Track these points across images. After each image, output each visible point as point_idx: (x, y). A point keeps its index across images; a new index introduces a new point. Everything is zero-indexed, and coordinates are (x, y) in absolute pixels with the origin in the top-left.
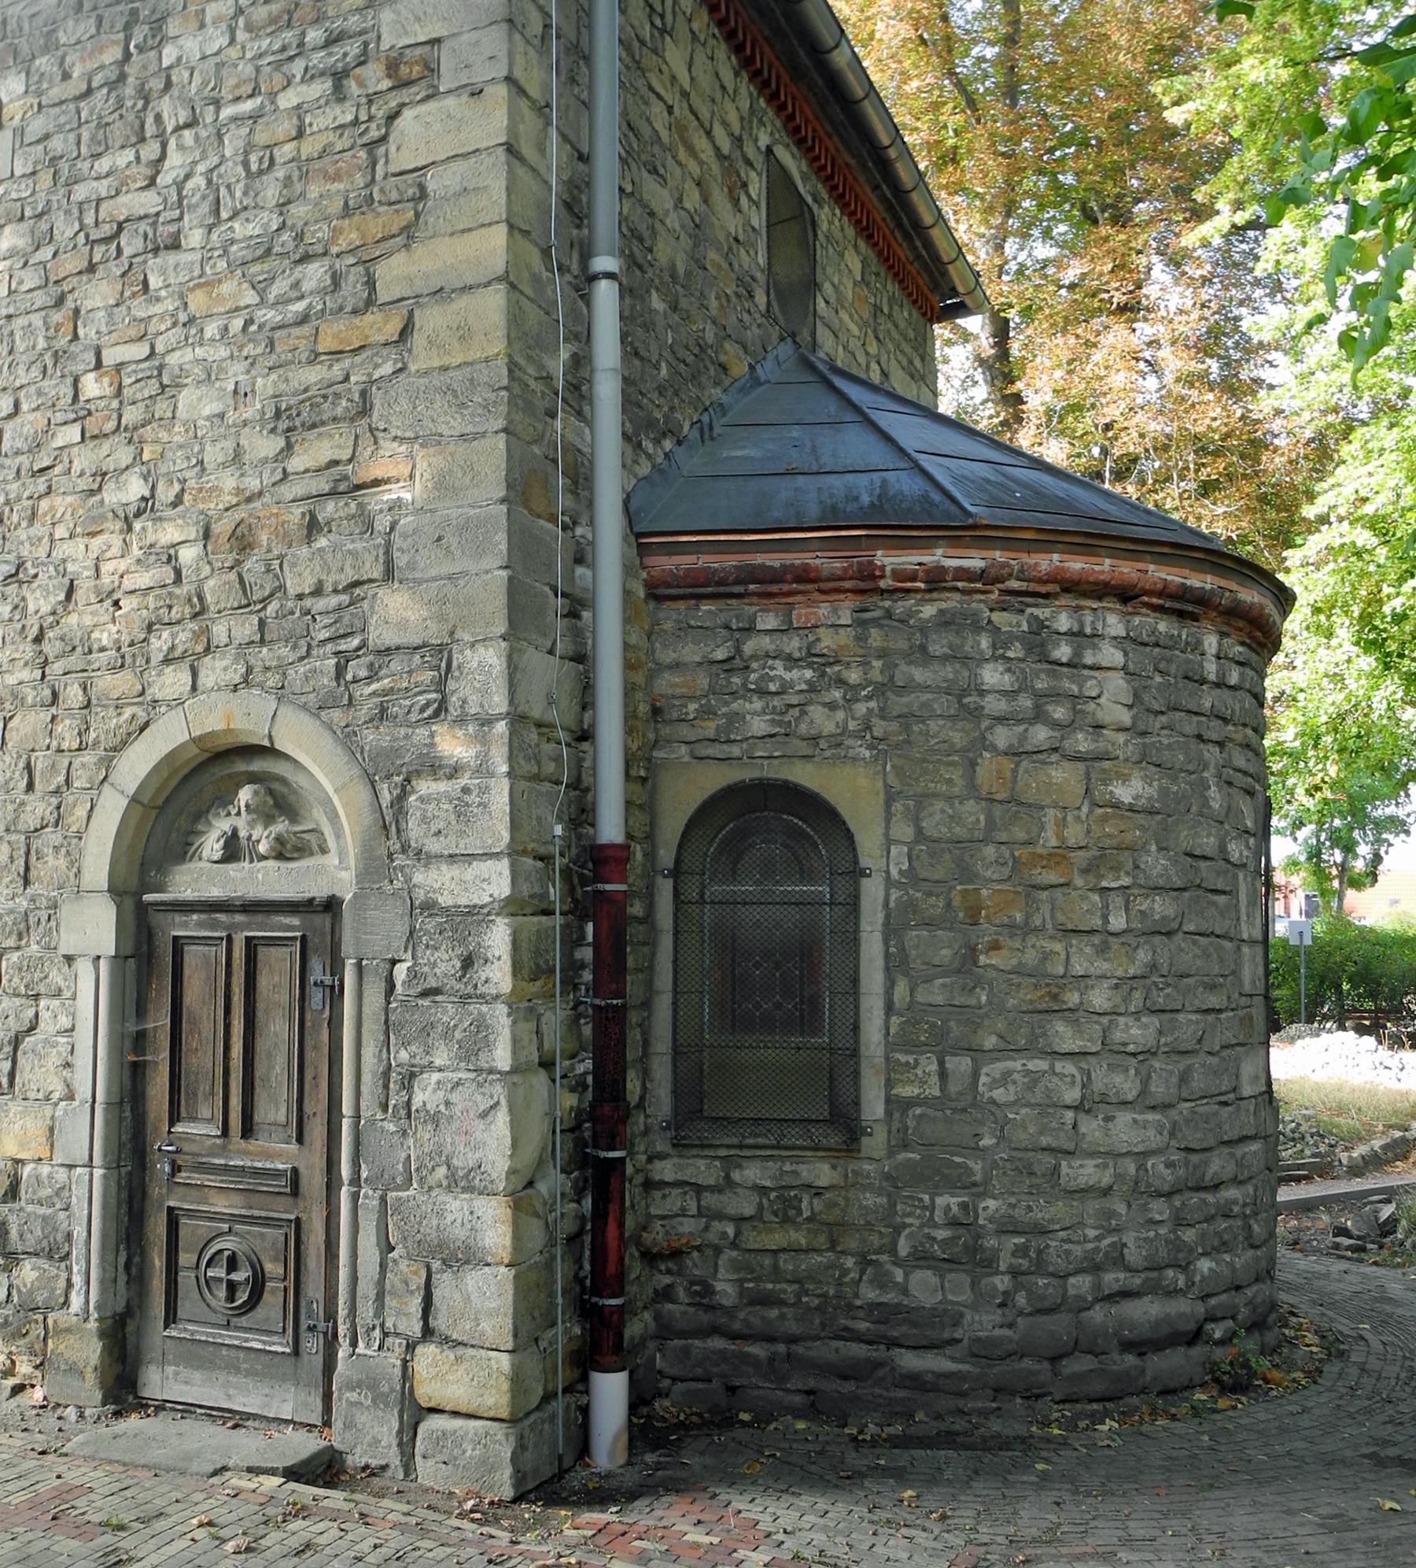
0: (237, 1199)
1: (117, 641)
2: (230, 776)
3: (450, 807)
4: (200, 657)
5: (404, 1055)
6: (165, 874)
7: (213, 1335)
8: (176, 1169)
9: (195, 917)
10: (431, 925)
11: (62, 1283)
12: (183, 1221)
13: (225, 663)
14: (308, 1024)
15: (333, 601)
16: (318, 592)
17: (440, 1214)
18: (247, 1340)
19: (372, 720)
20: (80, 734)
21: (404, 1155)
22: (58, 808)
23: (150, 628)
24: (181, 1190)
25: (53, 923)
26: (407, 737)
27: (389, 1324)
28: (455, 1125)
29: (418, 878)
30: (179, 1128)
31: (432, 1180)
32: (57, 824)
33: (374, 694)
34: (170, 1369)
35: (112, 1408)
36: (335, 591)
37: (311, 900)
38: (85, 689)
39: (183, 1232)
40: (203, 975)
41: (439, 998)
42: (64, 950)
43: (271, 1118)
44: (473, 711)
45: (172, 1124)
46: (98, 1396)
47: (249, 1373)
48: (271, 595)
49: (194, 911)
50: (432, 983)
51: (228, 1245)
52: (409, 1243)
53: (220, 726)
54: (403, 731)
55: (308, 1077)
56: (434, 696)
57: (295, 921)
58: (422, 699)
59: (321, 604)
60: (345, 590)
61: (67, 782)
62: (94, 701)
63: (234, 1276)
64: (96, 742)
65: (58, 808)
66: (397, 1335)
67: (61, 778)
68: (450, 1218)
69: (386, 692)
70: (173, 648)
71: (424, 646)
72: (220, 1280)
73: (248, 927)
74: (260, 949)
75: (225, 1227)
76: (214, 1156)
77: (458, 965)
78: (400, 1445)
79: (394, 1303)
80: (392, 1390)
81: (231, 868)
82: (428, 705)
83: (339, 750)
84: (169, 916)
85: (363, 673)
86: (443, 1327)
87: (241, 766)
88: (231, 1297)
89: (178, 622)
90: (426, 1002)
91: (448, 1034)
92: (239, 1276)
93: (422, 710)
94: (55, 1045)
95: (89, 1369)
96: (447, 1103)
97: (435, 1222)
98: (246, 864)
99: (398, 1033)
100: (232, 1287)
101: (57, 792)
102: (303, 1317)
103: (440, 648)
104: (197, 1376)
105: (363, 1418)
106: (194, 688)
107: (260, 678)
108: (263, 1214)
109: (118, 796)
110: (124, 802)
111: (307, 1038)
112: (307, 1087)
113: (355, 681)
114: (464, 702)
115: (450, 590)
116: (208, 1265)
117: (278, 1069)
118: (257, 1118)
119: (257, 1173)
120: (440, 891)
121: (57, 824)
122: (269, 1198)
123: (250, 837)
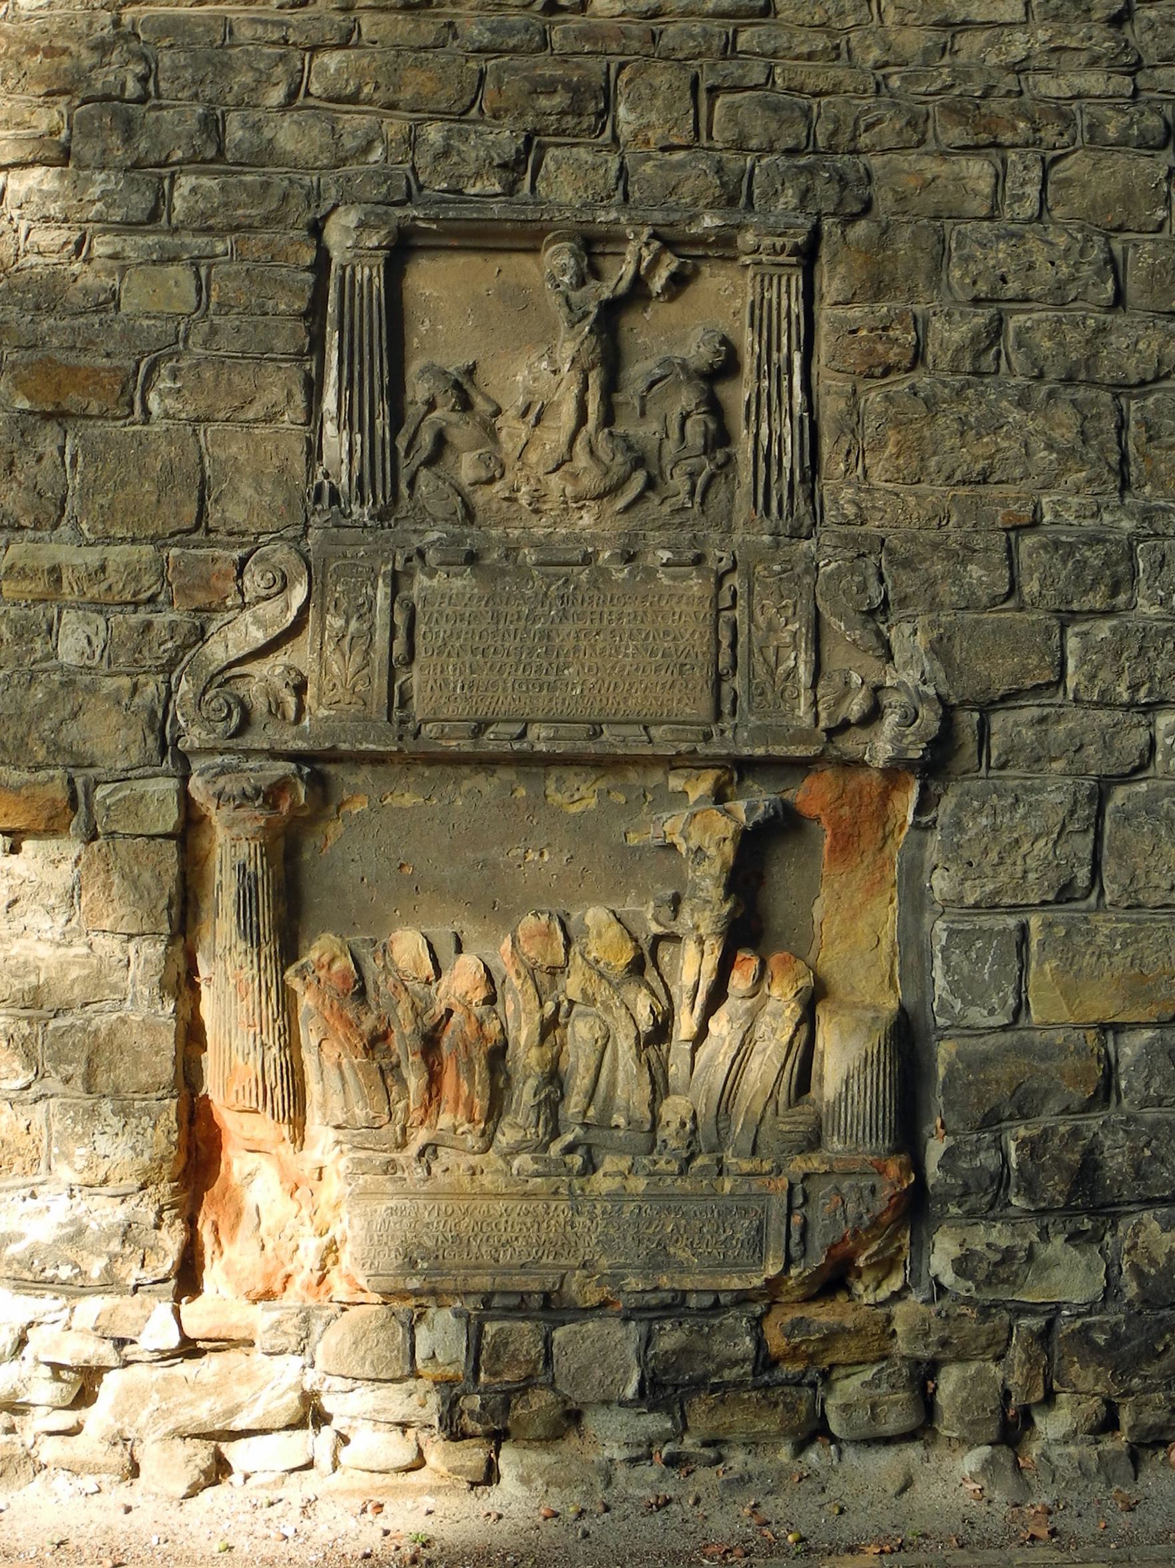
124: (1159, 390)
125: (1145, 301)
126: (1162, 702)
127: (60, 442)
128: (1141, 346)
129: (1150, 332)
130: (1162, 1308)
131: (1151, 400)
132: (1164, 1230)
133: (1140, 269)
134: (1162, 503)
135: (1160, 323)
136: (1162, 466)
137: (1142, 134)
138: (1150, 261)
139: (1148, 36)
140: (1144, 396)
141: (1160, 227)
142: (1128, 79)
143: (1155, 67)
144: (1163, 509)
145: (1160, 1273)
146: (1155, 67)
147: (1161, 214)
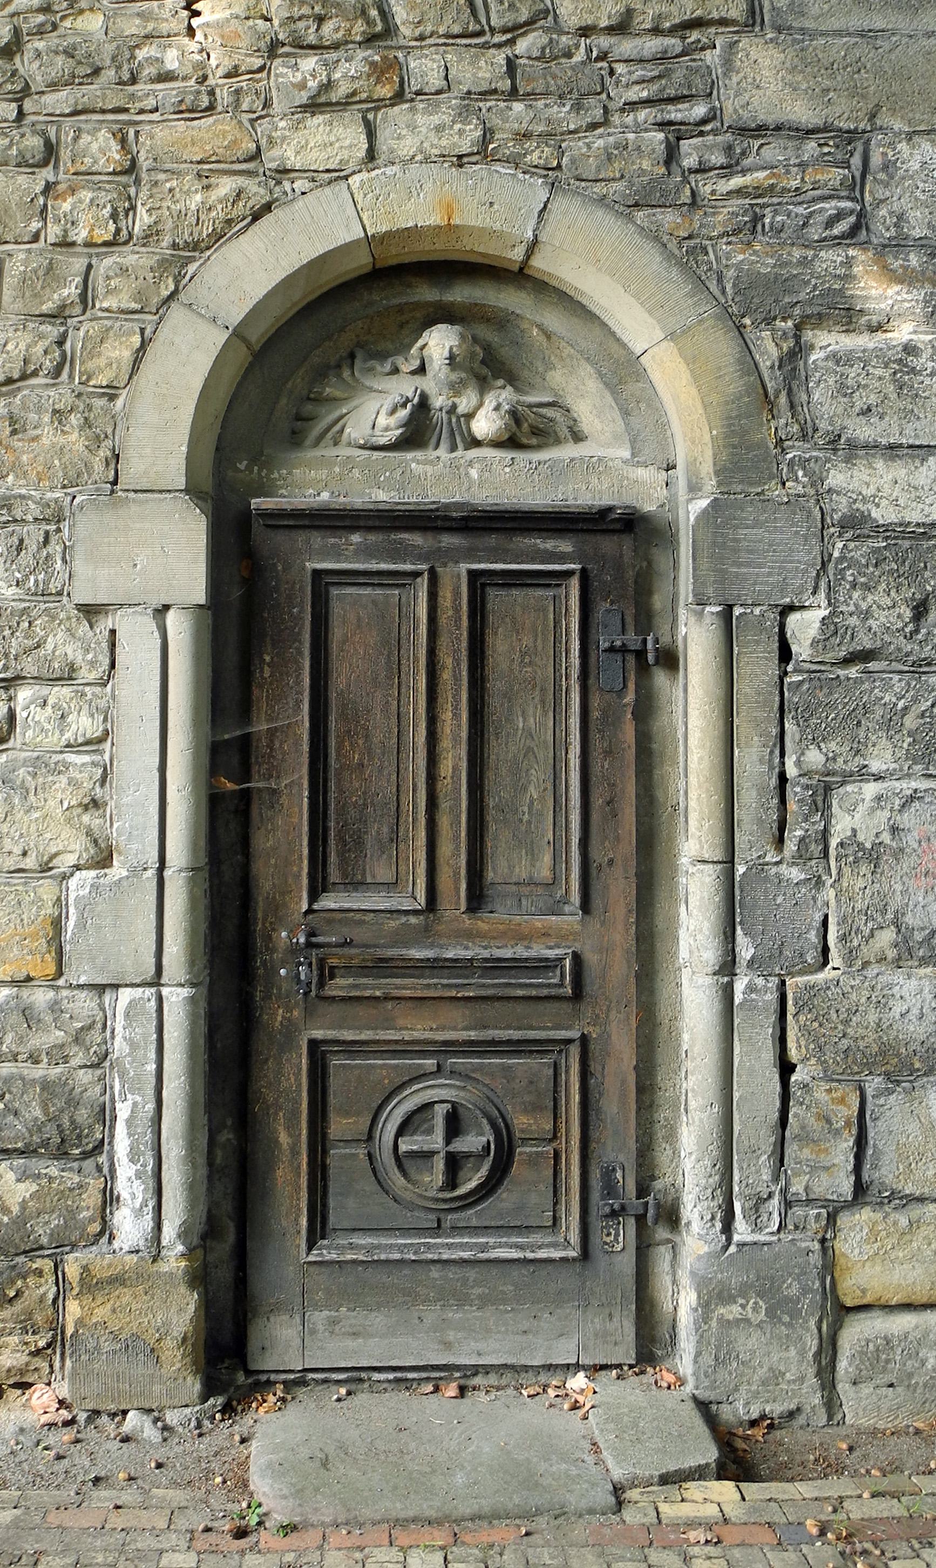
0: (457, 1014)
1: (201, 66)
2: (400, 309)
3: (887, 374)
4: (379, 104)
5: (814, 757)
6: (268, 464)
7: (416, 1249)
8: (325, 973)
9: (356, 538)
10: (860, 552)
11: (92, 1198)
12: (335, 1062)
13: (436, 119)
14: (595, 714)
15: (652, 45)
16: (621, 28)
17: (882, 1005)
18: (484, 1248)
19: (739, 231)
20: (114, 216)
21: (818, 917)
22: (60, 343)
23: (273, 49)
24: (334, 1011)
25: (55, 548)
26: (804, 262)
27: (797, 1187)
28: (906, 864)
29: (836, 478)
30: (328, 902)
31: (867, 952)
32: (57, 372)
33: (739, 192)
34: (319, 1318)
35: (217, 1401)
36: (656, 31)
37: (605, 512)
38: (123, 141)
39: (335, 1083)
40: (373, 638)
41: (872, 666)
42: (83, 596)
43: (521, 871)
44: (917, 233)
45: (314, 896)
46: (194, 1386)
47: (484, 1301)
48: (530, 23)
49: (354, 529)
50: (865, 642)
51: (444, 1094)
52: (829, 1057)
53: (434, 219)
54: (797, 253)
55: (597, 802)
56: (848, 204)
57: (565, 546)
58: (830, 207)
59: (626, 47)
60: (673, 31)
61: (84, 299)
62: (144, 162)
63: (461, 1145)
64: (152, 234)
65: (60, 343)
66: (809, 1202)
67: (71, 291)
68: (898, 1008)
69: (759, 191)
70: (328, 86)
71: (825, 129)
72: (427, 1155)
73: (470, 554)
74: (491, 593)
75: (430, 1063)
76: (406, 945)
77: (908, 614)
78: (819, 1374)
79: (806, 1153)
80: (805, 1291)
81: (414, 460)
82: (839, 216)
83: (675, 272)
84: (300, 538)
85: (717, 159)
86: (889, 1180)
87: (427, 293)
88: (452, 1182)
89: (336, 46)
90: (853, 672)
91: (892, 722)
92: (471, 1142)
93: (830, 223)
94: (60, 769)
95: (169, 1343)
96: (894, 830)
97: (872, 1017)
98: (442, 452)
99: (803, 722)
100: (454, 1163)
101: (58, 315)
102: (595, 1196)
103: (851, 136)
104: (378, 1320)
105: (752, 1343)
106: (371, 155)
107: (511, 148)
108: (516, 1035)
109: (204, 327)
110: (224, 336)
111: (595, 737)
112: (595, 817)
113: (702, 169)
114: (901, 217)
115: (863, 49)
116: (401, 1132)
117: (533, 792)
118: (490, 875)
119: (496, 966)
120: (874, 500)
121: (57, 372)
122: (520, 1008)
123: (453, 409)
124: (27, 387)
125: (18, 306)
126: (18, 678)
127: (392, 425)
128: (10, 347)
129: (19, 333)
130: (17, 1255)
131: (17, 400)
132: (18, 1180)
133: (12, 276)
134: (23, 491)
135: (31, 325)
136: (25, 458)
137: (21, 153)
138: (22, 268)
139: (36, 65)
140: (13, 393)
141: (36, 238)
142: (14, 105)
143: (43, 93)
144: (22, 497)
145: (14, 1221)
146: (43, 93)
147: (35, 225)
